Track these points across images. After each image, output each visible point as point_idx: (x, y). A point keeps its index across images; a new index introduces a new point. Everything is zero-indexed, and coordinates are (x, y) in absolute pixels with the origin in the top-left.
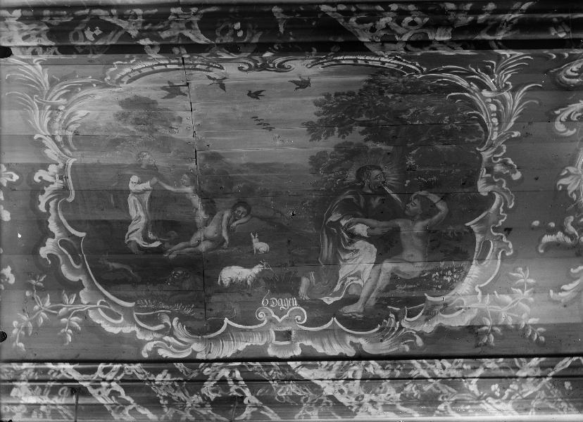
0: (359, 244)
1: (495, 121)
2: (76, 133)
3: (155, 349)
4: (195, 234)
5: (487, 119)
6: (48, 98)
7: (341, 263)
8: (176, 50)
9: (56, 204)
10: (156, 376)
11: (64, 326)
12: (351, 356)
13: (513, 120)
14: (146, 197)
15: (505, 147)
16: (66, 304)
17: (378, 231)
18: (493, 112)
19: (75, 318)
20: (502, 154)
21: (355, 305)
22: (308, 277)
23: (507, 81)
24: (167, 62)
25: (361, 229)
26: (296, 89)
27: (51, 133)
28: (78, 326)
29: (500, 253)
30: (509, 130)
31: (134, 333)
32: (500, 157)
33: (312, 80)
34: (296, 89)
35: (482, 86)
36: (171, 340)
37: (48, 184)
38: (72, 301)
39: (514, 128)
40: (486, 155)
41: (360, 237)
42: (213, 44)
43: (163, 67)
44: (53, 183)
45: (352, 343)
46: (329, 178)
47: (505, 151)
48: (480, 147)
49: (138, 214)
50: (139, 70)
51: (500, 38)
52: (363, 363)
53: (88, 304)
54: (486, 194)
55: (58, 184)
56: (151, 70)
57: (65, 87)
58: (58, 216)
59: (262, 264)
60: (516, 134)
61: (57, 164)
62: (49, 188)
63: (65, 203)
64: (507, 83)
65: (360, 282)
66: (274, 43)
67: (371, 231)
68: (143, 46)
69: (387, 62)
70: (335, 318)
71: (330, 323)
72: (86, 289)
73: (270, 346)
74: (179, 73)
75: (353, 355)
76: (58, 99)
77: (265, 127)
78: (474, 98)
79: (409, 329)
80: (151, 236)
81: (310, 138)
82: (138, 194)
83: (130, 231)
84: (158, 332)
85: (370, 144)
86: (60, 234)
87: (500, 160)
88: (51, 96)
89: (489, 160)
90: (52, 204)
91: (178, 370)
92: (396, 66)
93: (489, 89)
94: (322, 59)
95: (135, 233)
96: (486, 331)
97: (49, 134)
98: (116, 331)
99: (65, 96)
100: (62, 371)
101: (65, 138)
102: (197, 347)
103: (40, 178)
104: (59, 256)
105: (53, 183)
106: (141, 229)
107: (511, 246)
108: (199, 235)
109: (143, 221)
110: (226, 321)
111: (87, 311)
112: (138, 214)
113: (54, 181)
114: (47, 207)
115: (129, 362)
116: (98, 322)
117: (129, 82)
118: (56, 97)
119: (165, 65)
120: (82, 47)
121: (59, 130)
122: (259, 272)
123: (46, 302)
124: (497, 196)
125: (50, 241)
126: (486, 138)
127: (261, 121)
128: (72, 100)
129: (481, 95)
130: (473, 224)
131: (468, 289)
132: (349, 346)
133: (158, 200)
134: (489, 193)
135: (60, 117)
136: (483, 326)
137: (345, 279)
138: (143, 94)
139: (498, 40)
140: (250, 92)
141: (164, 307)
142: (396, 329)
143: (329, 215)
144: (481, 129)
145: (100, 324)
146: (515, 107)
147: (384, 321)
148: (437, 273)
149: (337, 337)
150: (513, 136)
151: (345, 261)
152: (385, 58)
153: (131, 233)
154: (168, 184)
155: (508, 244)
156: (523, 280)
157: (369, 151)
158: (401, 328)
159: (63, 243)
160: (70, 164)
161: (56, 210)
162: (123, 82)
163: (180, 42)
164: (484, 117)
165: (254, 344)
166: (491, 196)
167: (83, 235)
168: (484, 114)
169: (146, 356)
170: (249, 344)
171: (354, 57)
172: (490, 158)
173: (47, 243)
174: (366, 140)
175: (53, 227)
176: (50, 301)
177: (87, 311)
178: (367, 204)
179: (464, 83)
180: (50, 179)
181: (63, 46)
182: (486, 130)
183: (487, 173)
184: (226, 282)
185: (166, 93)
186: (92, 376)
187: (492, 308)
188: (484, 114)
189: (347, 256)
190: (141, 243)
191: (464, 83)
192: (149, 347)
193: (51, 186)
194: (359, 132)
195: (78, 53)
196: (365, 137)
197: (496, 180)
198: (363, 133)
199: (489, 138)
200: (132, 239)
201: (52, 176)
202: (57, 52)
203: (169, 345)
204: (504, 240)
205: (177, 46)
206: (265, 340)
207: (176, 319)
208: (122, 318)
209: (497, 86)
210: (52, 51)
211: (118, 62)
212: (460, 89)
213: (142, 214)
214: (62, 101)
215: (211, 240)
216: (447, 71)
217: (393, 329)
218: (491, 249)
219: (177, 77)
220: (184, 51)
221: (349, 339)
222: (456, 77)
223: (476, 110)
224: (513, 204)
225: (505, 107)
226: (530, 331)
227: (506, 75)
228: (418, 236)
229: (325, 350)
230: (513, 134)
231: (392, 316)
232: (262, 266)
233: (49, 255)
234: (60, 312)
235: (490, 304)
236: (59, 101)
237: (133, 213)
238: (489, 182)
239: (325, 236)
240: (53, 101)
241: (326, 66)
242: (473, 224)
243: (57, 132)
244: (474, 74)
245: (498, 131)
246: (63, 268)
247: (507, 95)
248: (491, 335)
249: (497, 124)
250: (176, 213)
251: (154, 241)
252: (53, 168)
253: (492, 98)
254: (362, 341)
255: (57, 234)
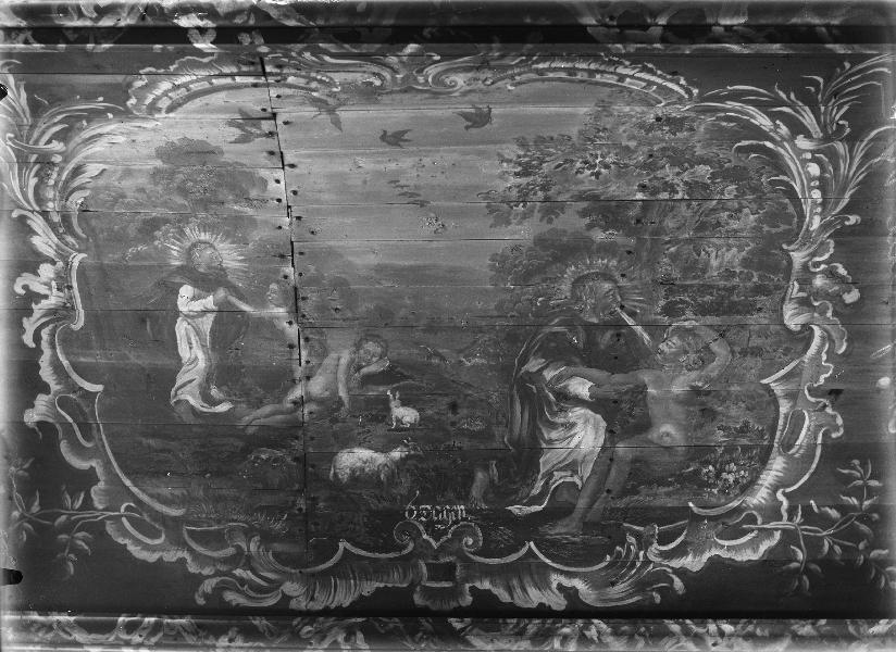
0: (577, 414)
1: (817, 195)
2: (84, 210)
3: (219, 589)
4: (213, 326)
5: (803, 192)
6: (31, 142)
7: (544, 445)
8: (246, 39)
9: (52, 335)
10: (217, 639)
11: (62, 547)
12: (558, 609)
13: (847, 195)
14: (207, 323)
15: (832, 243)
16: (67, 510)
17: (608, 391)
18: (814, 179)
19: (80, 535)
20: (826, 256)
21: (566, 521)
22: (486, 468)
23: (840, 119)
24: (235, 70)
25: (581, 388)
26: (467, 128)
27: (40, 206)
28: (86, 547)
29: (821, 435)
30: (840, 213)
31: (182, 561)
32: (823, 262)
33: (495, 111)
34: (467, 128)
35: (797, 128)
36: (247, 575)
37: (39, 297)
38: (78, 504)
39: (848, 210)
40: (798, 257)
41: (578, 401)
42: (313, 27)
43: (228, 80)
44: (46, 297)
45: (561, 587)
46: (525, 294)
47: (832, 251)
48: (789, 243)
49: (193, 354)
50: (185, 85)
51: (836, 22)
52: (580, 622)
53: (104, 510)
54: (799, 328)
55: (54, 300)
56: (206, 85)
57: (60, 117)
58: (55, 355)
59: (406, 446)
60: (853, 219)
61: (53, 263)
62: (40, 306)
63: (68, 333)
64: (841, 122)
65: (576, 480)
66: (423, 28)
67: (600, 391)
68: (186, 30)
69: (627, 76)
70: (532, 544)
71: (524, 551)
72: (101, 485)
73: (418, 589)
74: (259, 93)
75: (563, 608)
76: (49, 142)
77: (412, 199)
78: (782, 151)
79: (661, 565)
80: (214, 392)
81: (491, 221)
82: (193, 317)
83: (179, 382)
84: (225, 561)
85: (599, 236)
86: (58, 387)
87: (823, 266)
88: (35, 135)
89: (805, 267)
90: (45, 334)
91: (255, 627)
92: (644, 84)
93: (808, 135)
94: (512, 67)
95: (188, 388)
96: (797, 570)
97: (37, 209)
98: (152, 557)
99: (56, 137)
100: (55, 626)
101: (66, 218)
102: (290, 588)
103: (25, 287)
104: (57, 426)
105: (46, 297)
106: (198, 379)
107: (840, 421)
108: (298, 392)
109: (202, 364)
110: (342, 545)
111: (102, 523)
112: (193, 354)
113: (47, 292)
114: (37, 338)
115: (172, 613)
116: (121, 541)
117: (170, 109)
118: (46, 137)
119: (232, 75)
120: (76, 29)
121: (54, 200)
122: (401, 458)
123: (32, 505)
124: (817, 332)
125: (42, 401)
126: (800, 227)
127: (405, 189)
128: (72, 145)
129: (794, 147)
130: (775, 382)
131: (765, 495)
132: (557, 592)
133: (228, 330)
134: (803, 326)
135: (55, 176)
136: (791, 561)
137: (550, 475)
138: (196, 134)
139: (833, 26)
140: (385, 132)
141: (235, 518)
142: (638, 564)
143: (524, 361)
144: (791, 209)
145: (125, 545)
146: (854, 168)
147: (618, 548)
148: (711, 467)
149: (536, 577)
150: (847, 223)
151: (550, 441)
152: (626, 67)
153: (181, 387)
154: (241, 298)
155: (834, 417)
156: (861, 482)
157: (595, 247)
158: (647, 562)
159: (64, 403)
160: (76, 264)
161: (53, 347)
162: (159, 110)
163: (252, 22)
164: (798, 189)
165: (390, 585)
166: (807, 329)
167: (99, 388)
168: (798, 180)
169: (201, 601)
170: (382, 585)
171: (569, 65)
172: (806, 263)
173: (37, 403)
174: (590, 227)
175: (46, 373)
176: (40, 504)
177: (102, 523)
178: (591, 342)
179: (763, 121)
180: (42, 290)
181: (42, 28)
182: (802, 216)
183: (800, 290)
184: (344, 476)
185: (237, 132)
186: (107, 636)
187: (806, 530)
188: (798, 180)
189: (554, 435)
190: (195, 402)
191: (763, 121)
192: (208, 586)
193: (44, 302)
194: (578, 212)
195: (67, 42)
196: (587, 221)
197: (816, 304)
198: (584, 213)
199: (804, 227)
200: (182, 397)
201: (45, 284)
202: (31, 40)
203: (243, 586)
204: (829, 410)
205: (248, 30)
206: (411, 576)
207: (257, 538)
208: (163, 536)
209: (823, 128)
210: (22, 37)
211: (148, 69)
212: (759, 133)
213: (201, 355)
214: (57, 146)
215: (320, 401)
216: (736, 96)
217: (633, 565)
218: (805, 426)
219: (252, 100)
220: (259, 40)
221: (556, 579)
222: (751, 109)
223: (786, 174)
224: (844, 348)
225: (835, 169)
226: (874, 572)
227: (840, 107)
228: (678, 400)
229: (512, 598)
230: (849, 219)
231: (632, 540)
232: (405, 449)
233: (39, 423)
234: (56, 523)
235: (803, 524)
236: (49, 146)
237: (184, 351)
238: (804, 303)
239: (517, 397)
240: (41, 145)
241: (519, 83)
242: (775, 382)
243: (51, 205)
244: (783, 104)
245: (821, 214)
246: (64, 447)
247: (840, 147)
248: (805, 577)
249: (820, 201)
250: (265, 354)
251: (220, 402)
252: (46, 271)
253: (812, 152)
254: (578, 584)
255: (54, 387)
